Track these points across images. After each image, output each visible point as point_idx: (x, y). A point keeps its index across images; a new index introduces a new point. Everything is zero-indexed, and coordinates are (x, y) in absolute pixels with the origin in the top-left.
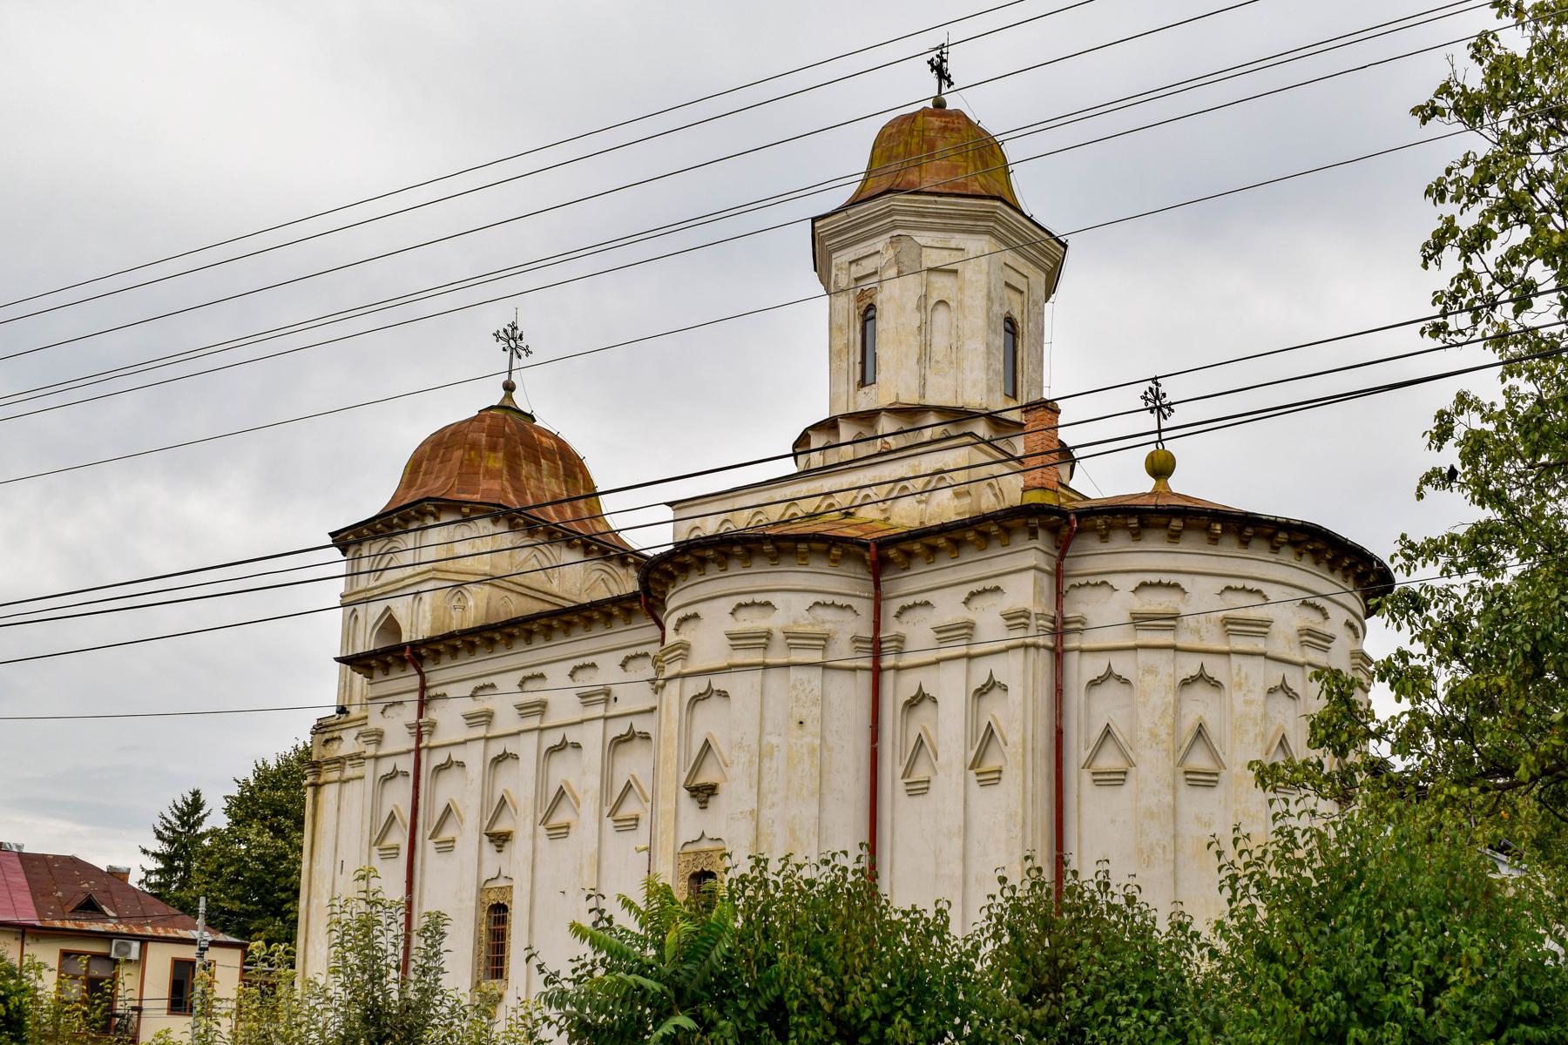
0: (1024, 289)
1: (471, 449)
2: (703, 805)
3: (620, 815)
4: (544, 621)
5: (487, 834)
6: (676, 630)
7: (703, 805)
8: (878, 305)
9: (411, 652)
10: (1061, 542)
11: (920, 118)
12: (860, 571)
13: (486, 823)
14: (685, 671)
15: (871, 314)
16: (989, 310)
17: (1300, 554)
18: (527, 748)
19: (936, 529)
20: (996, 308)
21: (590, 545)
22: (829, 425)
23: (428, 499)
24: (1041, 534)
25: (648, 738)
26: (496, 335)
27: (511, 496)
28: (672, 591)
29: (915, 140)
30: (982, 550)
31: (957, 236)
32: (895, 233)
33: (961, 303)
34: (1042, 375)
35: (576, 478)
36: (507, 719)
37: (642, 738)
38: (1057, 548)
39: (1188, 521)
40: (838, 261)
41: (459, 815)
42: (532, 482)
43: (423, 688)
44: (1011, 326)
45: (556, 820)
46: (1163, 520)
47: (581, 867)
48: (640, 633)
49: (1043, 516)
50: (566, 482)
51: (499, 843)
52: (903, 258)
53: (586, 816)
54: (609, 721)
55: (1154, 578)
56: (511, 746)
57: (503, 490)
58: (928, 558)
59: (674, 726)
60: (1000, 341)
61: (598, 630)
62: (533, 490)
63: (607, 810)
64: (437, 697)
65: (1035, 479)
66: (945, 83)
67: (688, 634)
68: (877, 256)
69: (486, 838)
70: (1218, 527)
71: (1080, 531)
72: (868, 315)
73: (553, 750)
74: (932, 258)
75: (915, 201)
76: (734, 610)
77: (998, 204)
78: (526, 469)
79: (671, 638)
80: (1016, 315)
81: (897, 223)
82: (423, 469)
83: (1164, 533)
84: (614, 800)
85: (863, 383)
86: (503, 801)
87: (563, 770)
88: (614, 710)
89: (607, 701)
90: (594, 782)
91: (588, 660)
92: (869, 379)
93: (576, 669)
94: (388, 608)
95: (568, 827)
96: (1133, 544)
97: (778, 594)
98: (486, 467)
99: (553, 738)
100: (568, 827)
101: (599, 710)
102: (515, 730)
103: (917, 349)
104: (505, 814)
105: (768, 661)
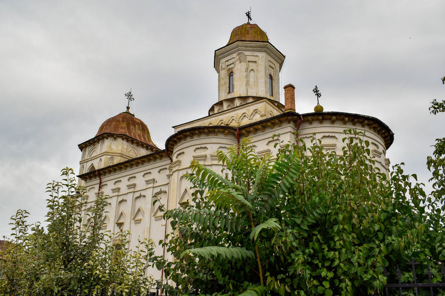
0: (274, 67)
1: (117, 122)
3: (156, 216)
4: (136, 161)
5: (116, 223)
6: (177, 158)
8: (234, 71)
9: (98, 172)
10: (297, 125)
11: (244, 25)
12: (233, 138)
13: (116, 220)
14: (179, 169)
15: (232, 74)
16: (265, 72)
17: (370, 128)
18: (129, 198)
19: (258, 122)
20: (267, 71)
21: (148, 147)
22: (220, 104)
23: (105, 133)
24: (291, 122)
25: (166, 193)
26: (126, 94)
27: (128, 134)
28: (175, 147)
29: (243, 30)
30: (272, 128)
31: (256, 52)
32: (240, 52)
33: (257, 70)
34: (279, 91)
35: (145, 130)
36: (124, 190)
37: (164, 193)
38: (296, 127)
39: (337, 117)
40: (222, 61)
41: (109, 219)
42: (133, 131)
43: (101, 183)
44: (271, 77)
45: (137, 218)
46: (330, 117)
47: (144, 232)
48: (165, 162)
49: (293, 116)
50: (142, 131)
51: (120, 226)
52: (241, 58)
53: (146, 217)
54: (154, 188)
55: (327, 134)
56: (124, 197)
57: (125, 132)
58: (255, 133)
59: (176, 186)
60: (268, 80)
61: (152, 162)
62: (133, 132)
63: (153, 214)
64: (104, 185)
65: (288, 107)
66: (250, 20)
67: (180, 158)
68: (234, 59)
69: (116, 225)
70: (347, 119)
71: (303, 121)
72: (231, 74)
73: (137, 198)
74: (249, 58)
75: (245, 43)
76: (195, 150)
77: (268, 43)
78: (132, 127)
79: (174, 159)
80: (272, 74)
81: (239, 49)
82: (104, 128)
83: (330, 121)
84: (155, 211)
85: (229, 92)
86: (122, 214)
87: (140, 204)
88: (156, 185)
89: (154, 183)
90: (149, 205)
91: (148, 171)
92: (231, 91)
93: (145, 174)
94: (92, 164)
95: (141, 220)
96: (320, 125)
97: (209, 144)
98: (121, 126)
99: (137, 194)
100: (141, 220)
101: (151, 185)
102: (126, 192)
103: (245, 82)
104: (122, 218)
105: (206, 164)
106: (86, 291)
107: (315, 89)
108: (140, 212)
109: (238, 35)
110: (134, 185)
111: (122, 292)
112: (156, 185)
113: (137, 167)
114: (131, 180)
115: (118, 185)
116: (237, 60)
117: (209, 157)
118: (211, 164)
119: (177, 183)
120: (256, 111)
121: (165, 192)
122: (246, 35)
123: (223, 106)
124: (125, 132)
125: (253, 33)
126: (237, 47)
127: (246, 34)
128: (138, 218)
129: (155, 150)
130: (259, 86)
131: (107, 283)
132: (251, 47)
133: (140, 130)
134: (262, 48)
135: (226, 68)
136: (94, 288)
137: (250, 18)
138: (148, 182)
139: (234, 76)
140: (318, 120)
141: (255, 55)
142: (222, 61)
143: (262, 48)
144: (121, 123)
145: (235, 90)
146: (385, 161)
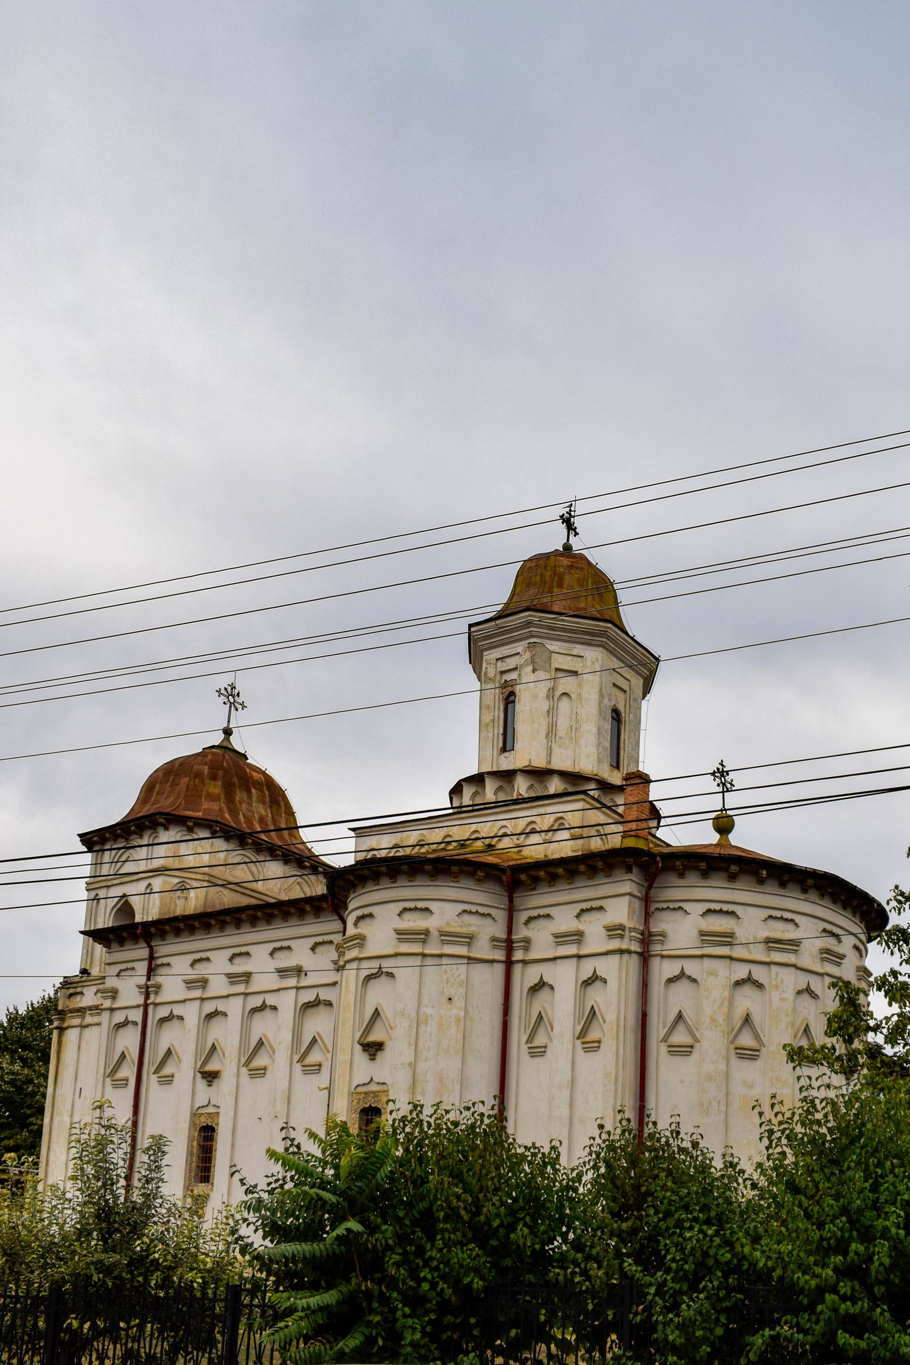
0: (627, 689)
2: (373, 1057)
5: (200, 1072)
7: (373, 1057)
8: (517, 692)
12: (498, 889)
13: (200, 1063)
14: (361, 956)
15: (512, 698)
16: (600, 703)
18: (234, 1008)
20: (606, 701)
22: (477, 780)
23: (160, 813)
24: (635, 870)
27: (227, 815)
28: (352, 896)
29: (549, 573)
31: (578, 646)
33: (579, 696)
35: (279, 805)
37: (326, 1004)
38: (646, 880)
40: (488, 657)
41: (178, 1057)
42: (244, 806)
43: (152, 958)
44: (616, 716)
46: (724, 865)
47: (275, 1100)
48: (327, 925)
50: (271, 807)
51: (210, 1079)
54: (301, 992)
55: (717, 907)
56: (221, 1006)
57: (221, 810)
60: (608, 726)
61: (293, 921)
62: (245, 811)
63: (296, 1058)
66: (572, 533)
68: (517, 657)
69: (199, 1075)
72: (509, 699)
73: (254, 1010)
74: (559, 661)
77: (610, 625)
78: (239, 795)
79: (351, 931)
80: (621, 707)
83: (725, 875)
84: (303, 1050)
85: (504, 749)
87: (262, 1026)
88: (304, 982)
89: (299, 976)
95: (265, 1069)
96: (702, 881)
99: (256, 1002)
100: (265, 1069)
101: (292, 982)
103: (546, 727)
105: (427, 951)
106: (141, 1279)
107: (718, 769)
108: (263, 1048)
109: (535, 584)
110: (247, 977)
111: (192, 1282)
112: (304, 982)
113: (253, 927)
114: (237, 960)
115: (202, 970)
116: (526, 664)
117: (434, 933)
118: (438, 952)
119: (356, 992)
120: (559, 826)
121: (329, 1004)
122: (555, 590)
123: (484, 786)
124: (221, 810)
125: (575, 585)
126: (529, 624)
127: (555, 585)
128: (257, 1063)
129: (308, 864)
130: (582, 742)
131: (170, 1268)
132: (565, 630)
133: (264, 803)
134: (592, 634)
135: (498, 677)
136: (152, 1275)
137: (575, 529)
138: (283, 972)
139: (518, 707)
140: (696, 868)
141: (575, 652)
142: (488, 657)
143: (594, 636)
144: (207, 781)
145: (517, 746)
146: (858, 971)
